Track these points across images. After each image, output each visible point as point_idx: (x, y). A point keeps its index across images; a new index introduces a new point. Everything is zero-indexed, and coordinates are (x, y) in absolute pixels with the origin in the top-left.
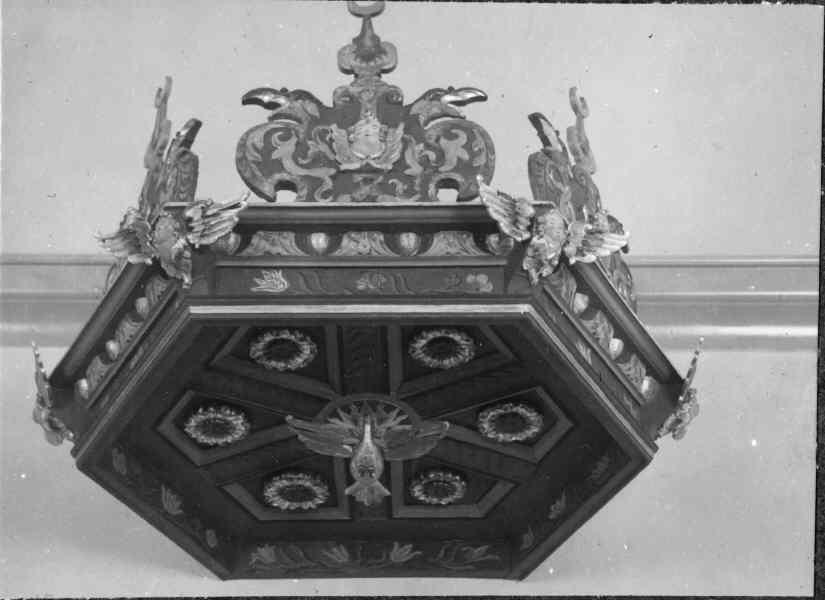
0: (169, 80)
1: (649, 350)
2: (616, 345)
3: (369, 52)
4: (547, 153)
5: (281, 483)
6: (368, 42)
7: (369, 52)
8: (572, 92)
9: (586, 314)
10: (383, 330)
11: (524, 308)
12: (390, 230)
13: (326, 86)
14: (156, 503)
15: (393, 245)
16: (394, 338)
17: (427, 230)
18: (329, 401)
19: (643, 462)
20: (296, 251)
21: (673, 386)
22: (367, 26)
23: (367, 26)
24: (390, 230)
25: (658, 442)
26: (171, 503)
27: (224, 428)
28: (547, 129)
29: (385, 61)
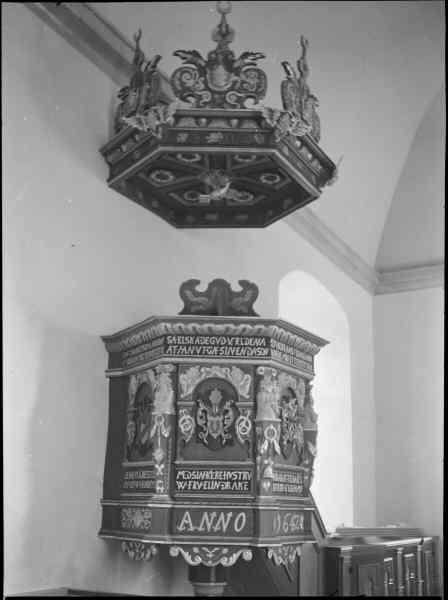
0: (140, 32)
1: (323, 156)
2: (310, 156)
3: (224, 34)
4: (289, 79)
5: (157, 172)
6: (224, 29)
7: (224, 34)
8: (302, 38)
9: (301, 148)
10: (225, 157)
11: (274, 151)
12: (228, 119)
13: (206, 47)
14: (136, 196)
15: (229, 124)
16: (228, 157)
17: (241, 119)
18: (328, 342)
19: (315, 433)
20: (194, 125)
21: (328, 171)
22: (224, 17)
23: (224, 17)
24: (228, 119)
25: (322, 189)
26: (155, 204)
27: (165, 178)
28: (288, 68)
29: (228, 38)
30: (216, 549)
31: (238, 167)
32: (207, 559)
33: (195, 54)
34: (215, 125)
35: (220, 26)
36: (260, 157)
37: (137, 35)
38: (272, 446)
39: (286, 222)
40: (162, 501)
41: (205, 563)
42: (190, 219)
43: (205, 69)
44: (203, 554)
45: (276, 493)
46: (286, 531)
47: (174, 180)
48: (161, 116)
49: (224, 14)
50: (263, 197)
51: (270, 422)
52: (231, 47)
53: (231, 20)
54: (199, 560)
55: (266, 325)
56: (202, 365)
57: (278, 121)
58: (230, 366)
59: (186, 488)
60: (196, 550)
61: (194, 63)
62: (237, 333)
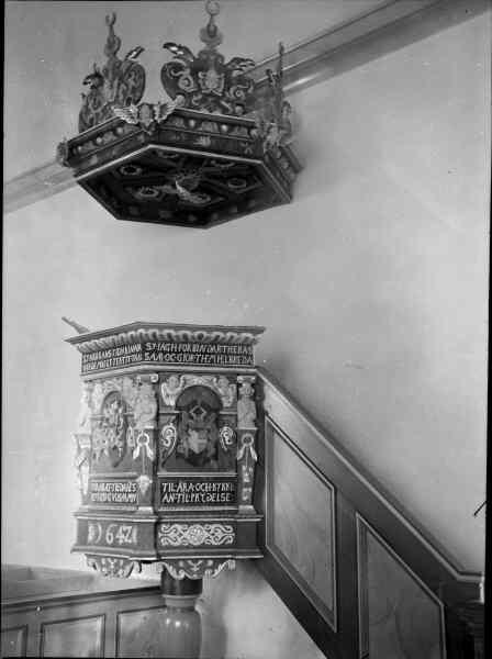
7: (211, 34)
13: (197, 47)
22: (211, 20)
23: (211, 20)
30: (200, 562)
31: (211, 169)
32: (192, 573)
33: (186, 50)
34: (208, 127)
35: (209, 26)
36: (237, 163)
37: (111, 18)
38: (247, 451)
39: (10, 211)
40: (248, 514)
41: (189, 577)
42: (134, 211)
43: (198, 67)
44: (187, 568)
45: (97, 502)
46: (110, 542)
47: (143, 173)
48: (157, 113)
49: (212, 15)
50: (221, 199)
51: (246, 431)
52: (220, 49)
53: (219, 22)
54: (182, 575)
55: (208, 332)
56: (180, 373)
57: (138, 117)
58: (217, 374)
59: (176, 501)
60: (181, 564)
61: (184, 60)
62: (240, 342)
